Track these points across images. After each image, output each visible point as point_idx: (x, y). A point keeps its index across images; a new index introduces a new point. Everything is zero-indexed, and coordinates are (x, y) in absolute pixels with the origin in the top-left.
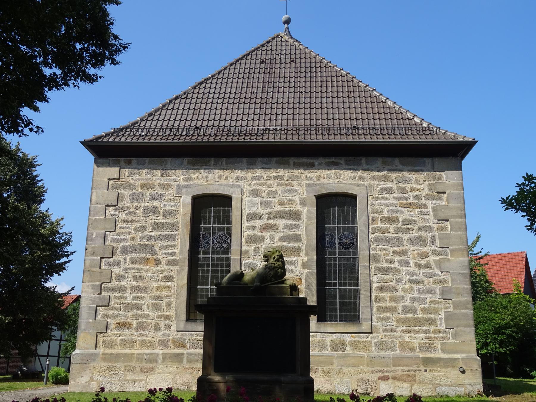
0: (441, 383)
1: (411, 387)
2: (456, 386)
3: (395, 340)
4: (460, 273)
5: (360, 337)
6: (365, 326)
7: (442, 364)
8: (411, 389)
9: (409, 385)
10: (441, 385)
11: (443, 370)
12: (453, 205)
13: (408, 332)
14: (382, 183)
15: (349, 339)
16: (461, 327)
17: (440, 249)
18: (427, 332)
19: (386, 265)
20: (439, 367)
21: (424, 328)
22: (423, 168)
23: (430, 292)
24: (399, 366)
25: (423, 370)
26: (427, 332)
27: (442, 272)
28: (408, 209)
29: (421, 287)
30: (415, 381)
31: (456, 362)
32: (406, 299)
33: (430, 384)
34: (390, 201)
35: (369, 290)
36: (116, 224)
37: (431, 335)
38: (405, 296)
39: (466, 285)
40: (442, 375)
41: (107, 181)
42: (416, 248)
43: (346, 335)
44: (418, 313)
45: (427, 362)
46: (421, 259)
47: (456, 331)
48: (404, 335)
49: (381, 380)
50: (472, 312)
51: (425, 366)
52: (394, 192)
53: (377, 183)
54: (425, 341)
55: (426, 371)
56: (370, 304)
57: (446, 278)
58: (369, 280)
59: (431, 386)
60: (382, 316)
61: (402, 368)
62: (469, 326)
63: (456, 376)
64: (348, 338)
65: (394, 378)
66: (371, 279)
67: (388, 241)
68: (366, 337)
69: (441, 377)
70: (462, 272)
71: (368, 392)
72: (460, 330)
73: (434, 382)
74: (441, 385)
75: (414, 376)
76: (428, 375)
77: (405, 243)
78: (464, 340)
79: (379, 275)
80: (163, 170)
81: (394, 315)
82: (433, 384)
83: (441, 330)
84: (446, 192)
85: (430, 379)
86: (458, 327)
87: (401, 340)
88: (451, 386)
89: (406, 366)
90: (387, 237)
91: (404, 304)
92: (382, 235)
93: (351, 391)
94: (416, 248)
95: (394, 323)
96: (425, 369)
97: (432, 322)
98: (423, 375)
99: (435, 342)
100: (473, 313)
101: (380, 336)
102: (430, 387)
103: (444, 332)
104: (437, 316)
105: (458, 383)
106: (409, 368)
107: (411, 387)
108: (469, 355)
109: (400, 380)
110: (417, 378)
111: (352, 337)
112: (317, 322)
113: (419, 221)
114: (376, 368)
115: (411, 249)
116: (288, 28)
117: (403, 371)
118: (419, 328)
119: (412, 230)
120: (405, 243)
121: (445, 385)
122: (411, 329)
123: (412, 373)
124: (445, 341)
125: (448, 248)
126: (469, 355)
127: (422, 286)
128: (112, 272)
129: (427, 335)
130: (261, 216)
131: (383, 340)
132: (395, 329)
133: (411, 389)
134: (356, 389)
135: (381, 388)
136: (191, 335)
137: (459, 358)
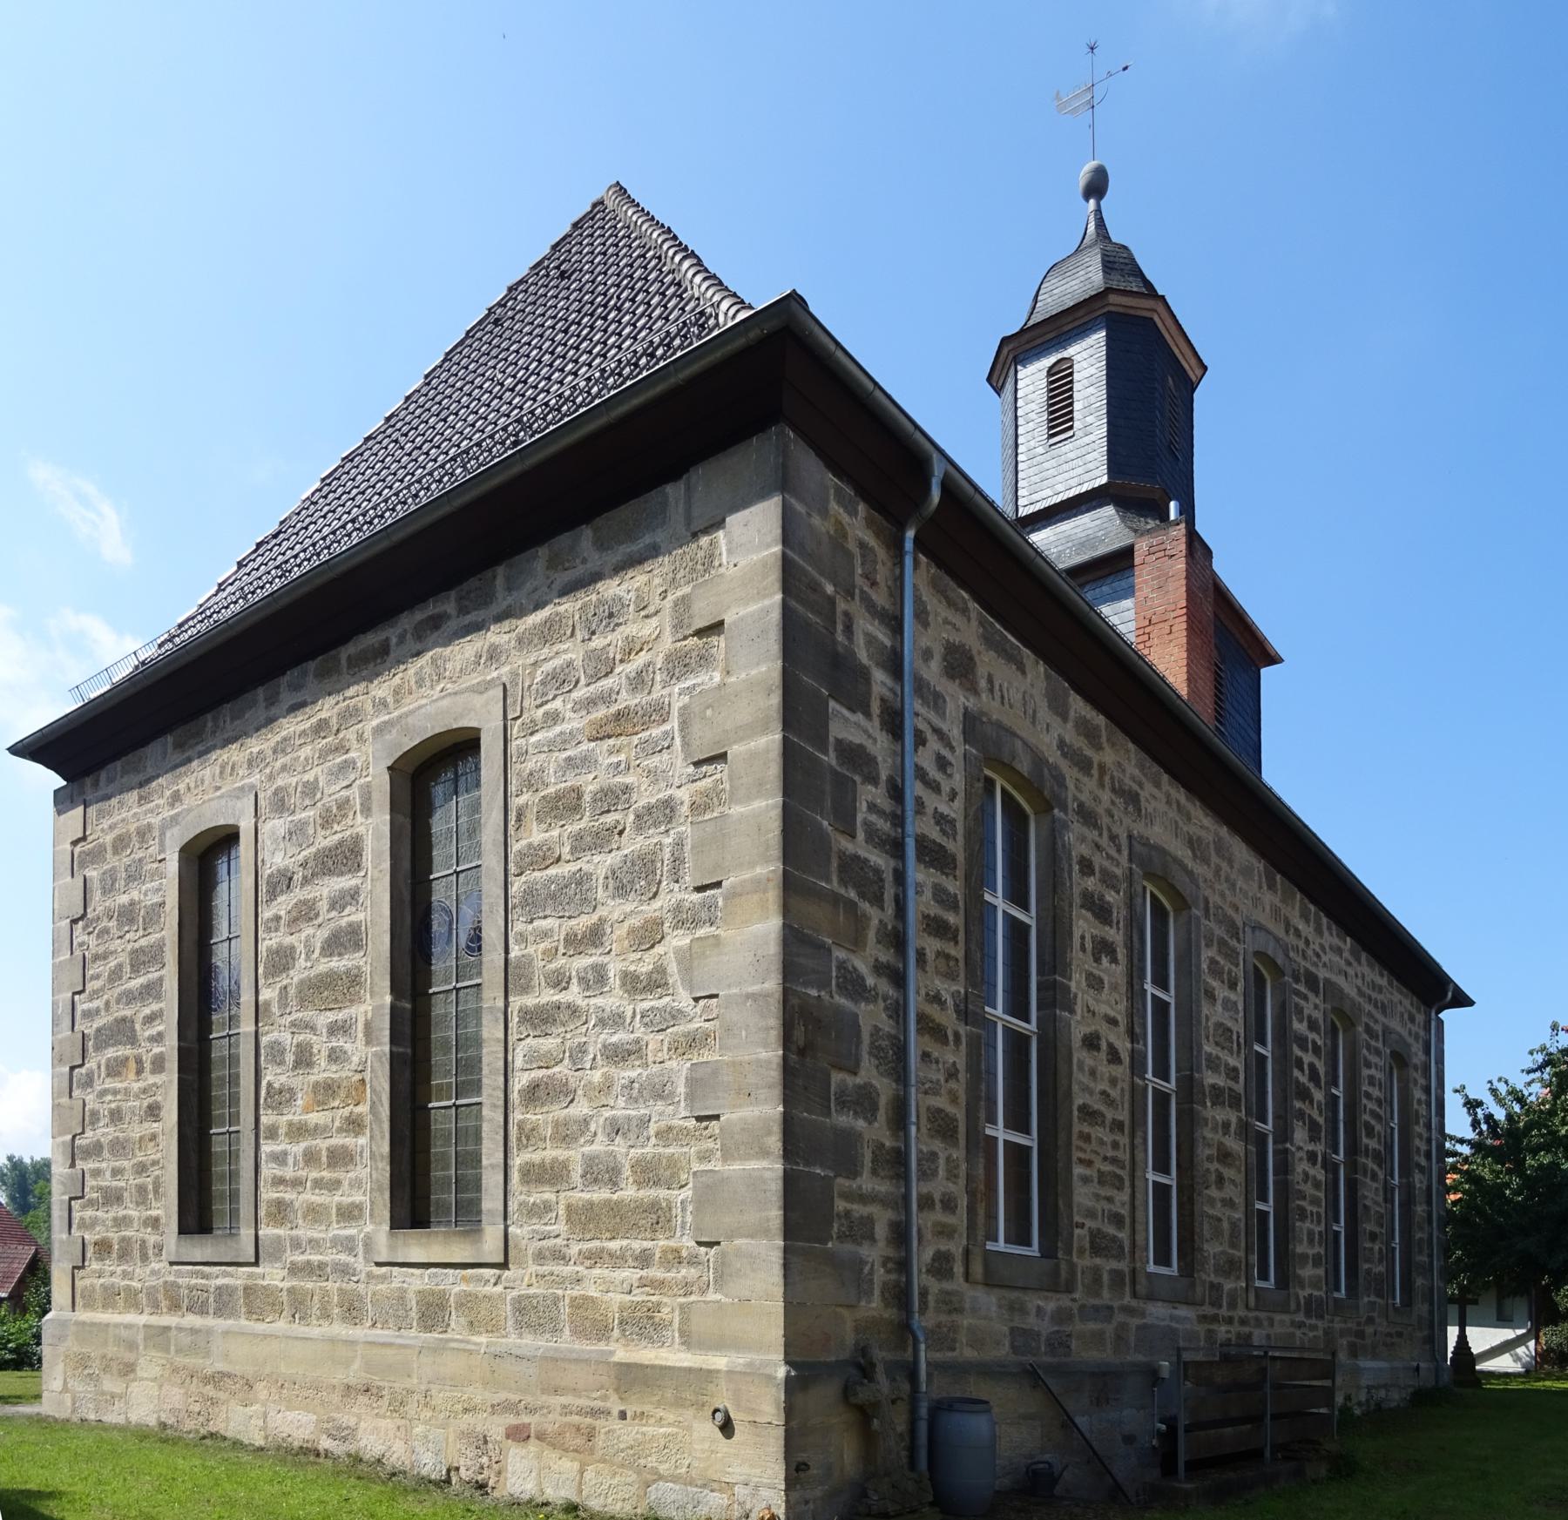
0: (663, 1468)
1: (582, 1472)
2: (704, 1486)
3: (560, 1292)
4: (748, 996)
5: (479, 1279)
6: (490, 1246)
7: (669, 1394)
8: (580, 1483)
9: (576, 1465)
10: (661, 1478)
11: (671, 1417)
12: (743, 676)
13: (594, 1258)
14: (545, 652)
15: (456, 1289)
16: (742, 1236)
17: (697, 897)
18: (644, 1259)
19: (549, 996)
20: (658, 1404)
21: (637, 1245)
22: (660, 536)
23: (659, 1091)
24: (556, 1391)
25: (615, 1413)
26: (644, 1259)
27: (696, 1000)
28: (611, 742)
29: (633, 1074)
30: (592, 1451)
31: (711, 1387)
32: (593, 1127)
33: (630, 1466)
34: (676, 728)
35: (501, 1102)
36: (1054, 932)
37: (656, 1273)
38: (593, 1116)
39: (765, 1045)
40: (665, 1436)
41: (68, 847)
42: (628, 907)
43: (450, 1271)
44: (623, 1186)
45: (632, 1378)
46: (639, 955)
47: (724, 1254)
48: (586, 1272)
49: (514, 1440)
50: (779, 1167)
51: (621, 1399)
52: (577, 682)
53: (532, 660)
54: (639, 1296)
55: (623, 1416)
56: (501, 1155)
57: (707, 1025)
58: (501, 1063)
59: (634, 1476)
60: (532, 1200)
61: (563, 1400)
62: (763, 1232)
63: (706, 1446)
64: (454, 1284)
65: (541, 1437)
66: (510, 1058)
67: (553, 897)
68: (493, 1281)
69: (662, 1446)
70: (755, 988)
71: (480, 1478)
72: (739, 1253)
73: (642, 1462)
74: (661, 1478)
75: (590, 1435)
76: (628, 1433)
77: (601, 894)
78: (747, 1294)
79: (529, 1040)
80: (141, 785)
81: (562, 1195)
82: (639, 1470)
83: (684, 1253)
84: (721, 623)
85: (632, 1447)
86: (730, 1238)
87: (577, 1292)
88: (691, 1484)
89: (575, 1391)
90: (551, 881)
91: (587, 1149)
92: (537, 874)
93: (444, 1472)
94: (628, 907)
95: (561, 1227)
96: (622, 1408)
97: (657, 1217)
98: (613, 1431)
99: (665, 1300)
100: (780, 1173)
101: (523, 1279)
102: (629, 1480)
103: (693, 1261)
104: (676, 1192)
105: (712, 1474)
106: (583, 1402)
107: (582, 1472)
108: (756, 1357)
109: (554, 1446)
110: (600, 1441)
111: (463, 1278)
112: (392, 1228)
113: (639, 786)
114: (502, 1396)
115: (615, 916)
116: (1100, 223)
117: (566, 1410)
118: (625, 1242)
119: (621, 833)
120: (601, 894)
121: (674, 1479)
122: (602, 1250)
123: (588, 1420)
124: (692, 1298)
125: (718, 884)
126: (756, 1357)
127: (639, 1070)
128: (84, 1105)
129: (644, 1273)
130: (291, 879)
131: (532, 1291)
132: (564, 1250)
133: (580, 1483)
134: (456, 1465)
135: (510, 1468)
136: (192, 1274)
137: (718, 1371)
